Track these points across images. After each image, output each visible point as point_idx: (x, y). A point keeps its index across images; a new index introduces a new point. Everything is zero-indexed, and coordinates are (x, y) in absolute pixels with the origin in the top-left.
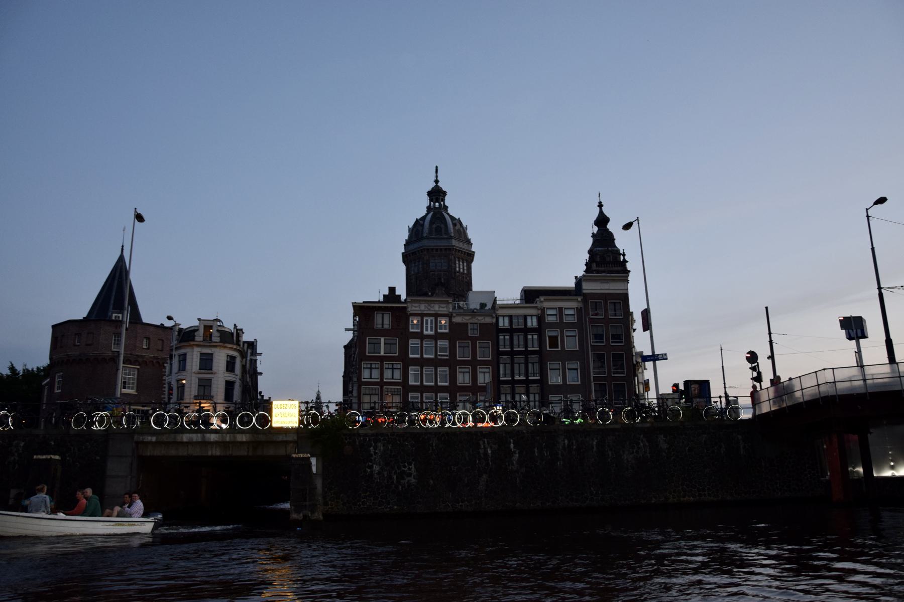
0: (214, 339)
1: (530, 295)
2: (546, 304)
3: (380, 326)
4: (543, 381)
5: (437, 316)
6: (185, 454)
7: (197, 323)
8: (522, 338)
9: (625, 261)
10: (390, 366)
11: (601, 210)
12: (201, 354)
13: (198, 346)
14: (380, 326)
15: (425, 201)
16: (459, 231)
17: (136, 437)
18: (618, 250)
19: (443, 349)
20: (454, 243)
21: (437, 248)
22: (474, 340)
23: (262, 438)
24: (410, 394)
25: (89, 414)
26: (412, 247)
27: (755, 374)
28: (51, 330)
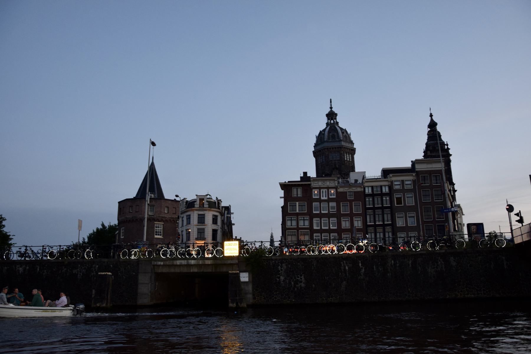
0: (205, 206)
1: (386, 172)
2: (394, 179)
3: (296, 196)
4: (393, 225)
5: (328, 188)
6: (179, 271)
7: (195, 197)
8: (379, 199)
9: (448, 149)
10: (303, 218)
11: (432, 118)
12: (199, 215)
13: (196, 210)
14: (296, 196)
15: (325, 120)
16: (345, 136)
17: (153, 262)
18: (444, 142)
19: (333, 208)
20: (343, 143)
21: (333, 148)
22: (351, 201)
23: (219, 262)
24: (314, 235)
25: (129, 250)
26: (318, 148)
27: (518, 218)
28: (118, 204)
